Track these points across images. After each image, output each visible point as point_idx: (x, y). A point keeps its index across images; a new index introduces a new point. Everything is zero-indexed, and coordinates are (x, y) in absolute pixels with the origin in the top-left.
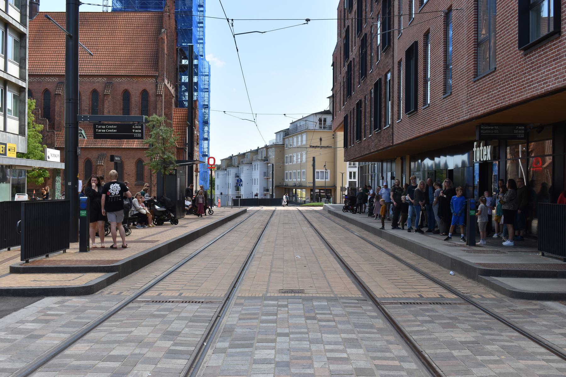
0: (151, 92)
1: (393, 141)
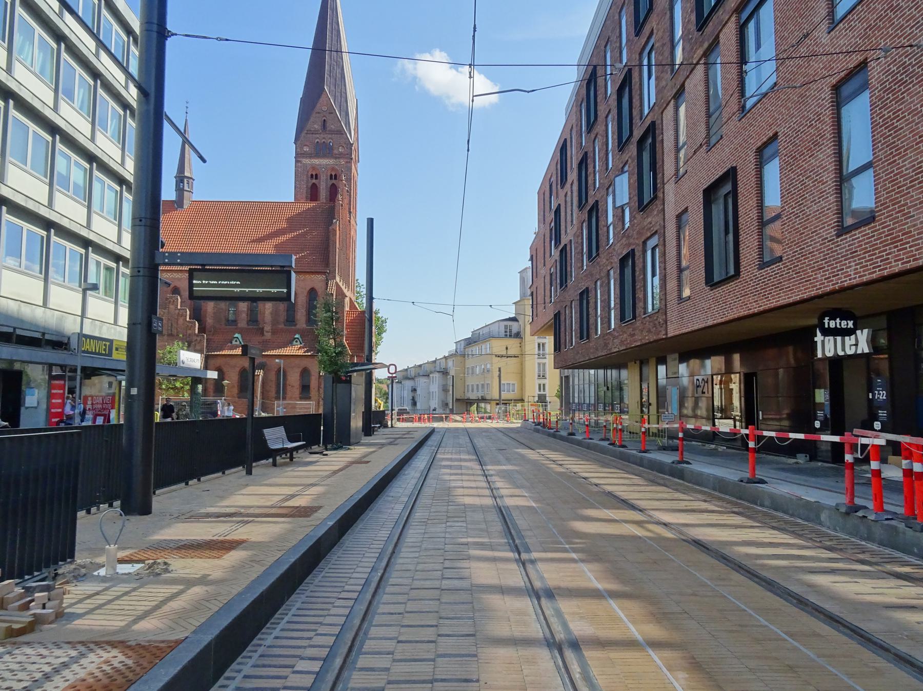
0: (320, 291)
1: (667, 332)
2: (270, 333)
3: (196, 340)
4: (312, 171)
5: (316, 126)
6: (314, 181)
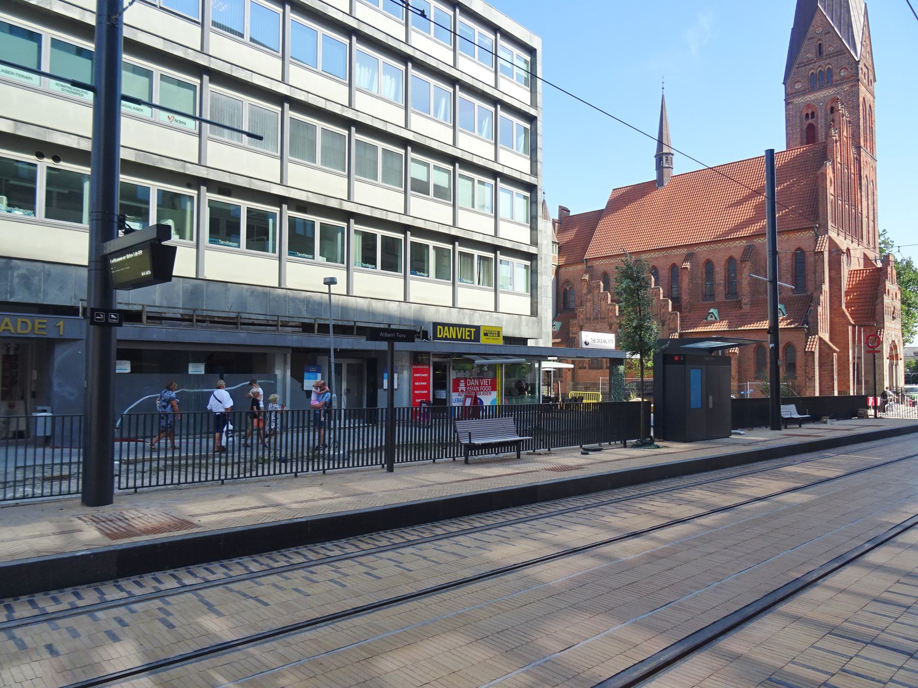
2: (749, 306)
3: (670, 318)
4: (807, 109)
5: (809, 55)
6: (810, 121)
